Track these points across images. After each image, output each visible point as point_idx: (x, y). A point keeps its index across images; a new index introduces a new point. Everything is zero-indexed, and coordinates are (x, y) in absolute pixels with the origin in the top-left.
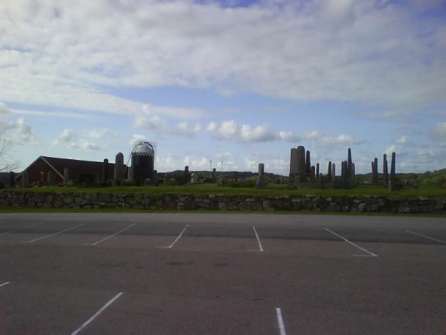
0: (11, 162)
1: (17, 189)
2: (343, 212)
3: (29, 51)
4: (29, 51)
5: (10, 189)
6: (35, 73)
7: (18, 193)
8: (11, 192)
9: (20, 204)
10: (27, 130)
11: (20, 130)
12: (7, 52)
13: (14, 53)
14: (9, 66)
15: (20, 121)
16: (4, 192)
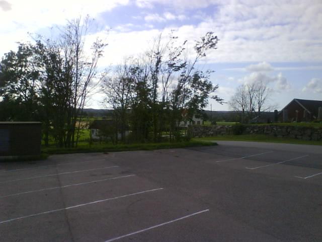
0: (272, 103)
1: (279, 123)
2: (160, 144)
3: (288, 23)
4: (288, 23)
5: (275, 124)
6: (291, 39)
7: (282, 127)
8: (276, 126)
9: (283, 136)
10: (284, 81)
11: (279, 82)
12: (273, 27)
13: (277, 27)
14: (273, 37)
15: (280, 76)
16: (270, 126)
